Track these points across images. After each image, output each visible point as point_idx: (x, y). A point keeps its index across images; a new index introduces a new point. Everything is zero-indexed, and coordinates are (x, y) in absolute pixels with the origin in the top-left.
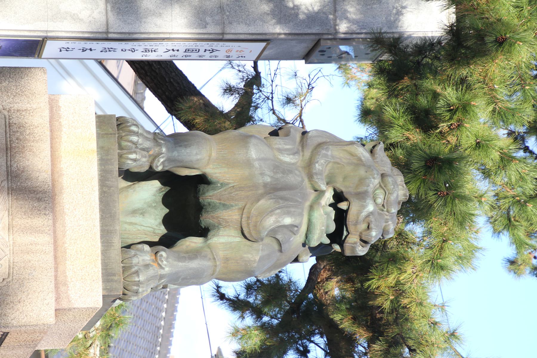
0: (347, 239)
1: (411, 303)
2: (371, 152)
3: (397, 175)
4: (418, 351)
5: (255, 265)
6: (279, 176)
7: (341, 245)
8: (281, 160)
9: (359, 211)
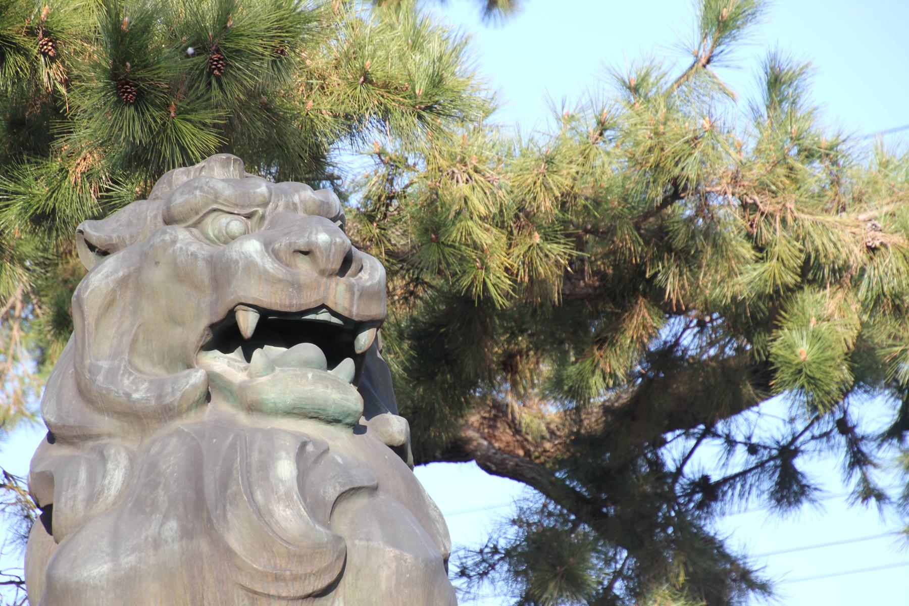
0: (339, 310)
1: (548, 189)
2: (104, 253)
3: (170, 184)
4: (677, 171)
5: (409, 557)
6: (162, 496)
7: (359, 326)
8: (120, 494)
9: (262, 276)
